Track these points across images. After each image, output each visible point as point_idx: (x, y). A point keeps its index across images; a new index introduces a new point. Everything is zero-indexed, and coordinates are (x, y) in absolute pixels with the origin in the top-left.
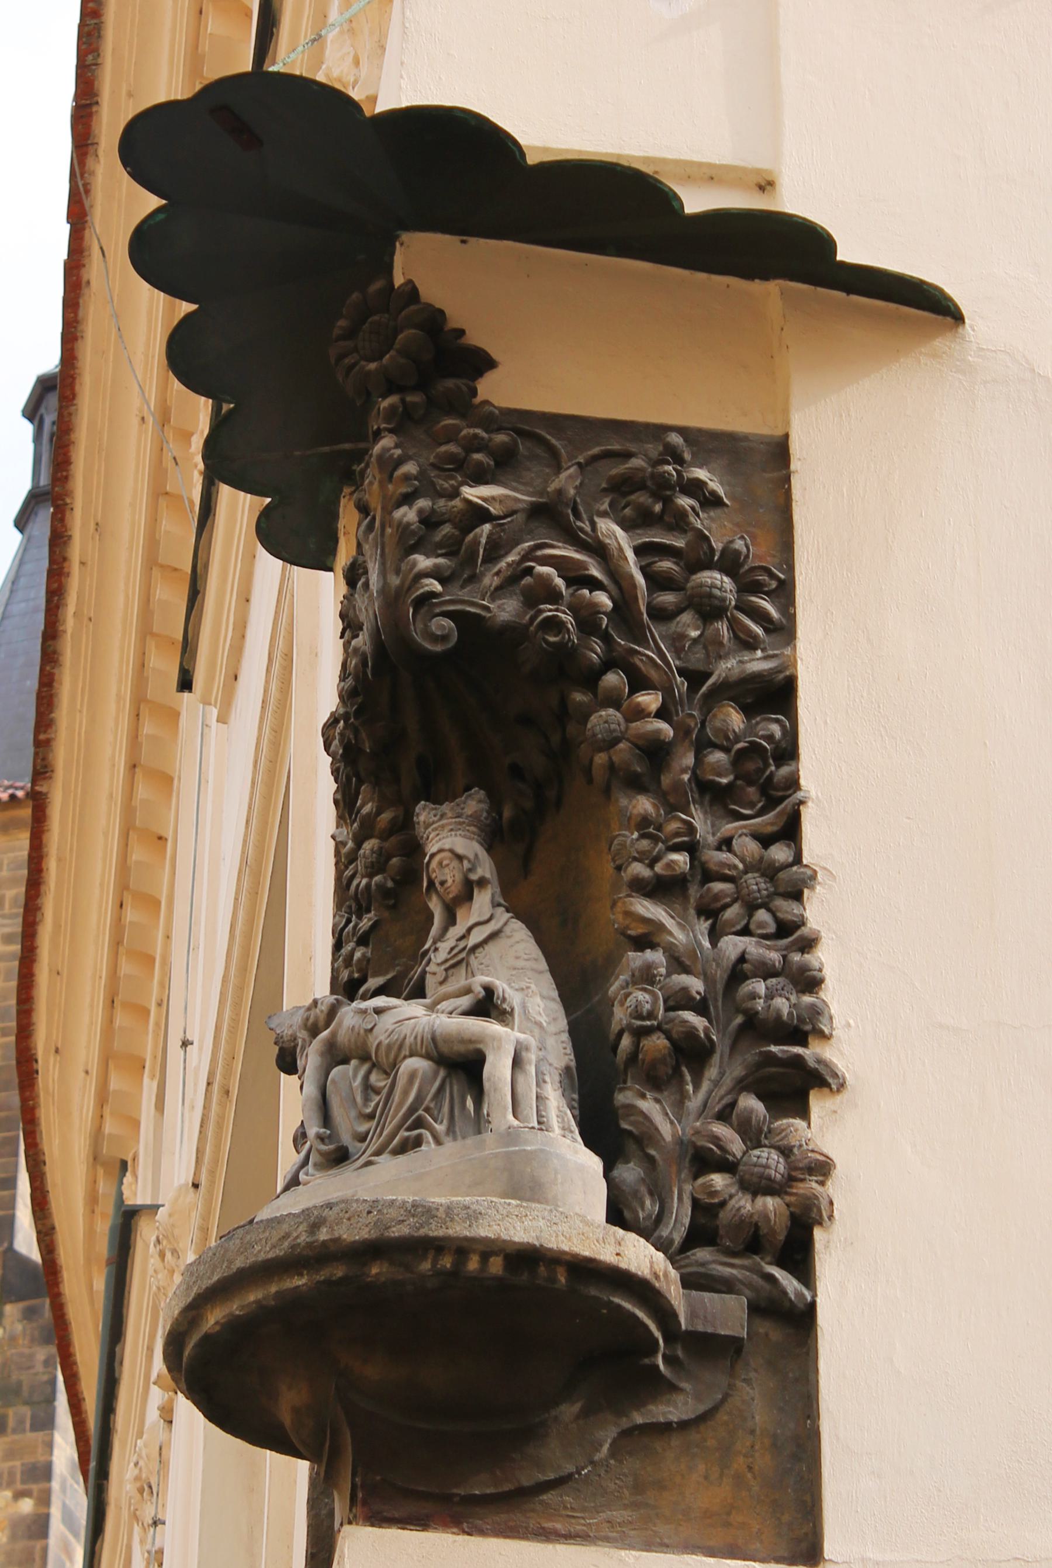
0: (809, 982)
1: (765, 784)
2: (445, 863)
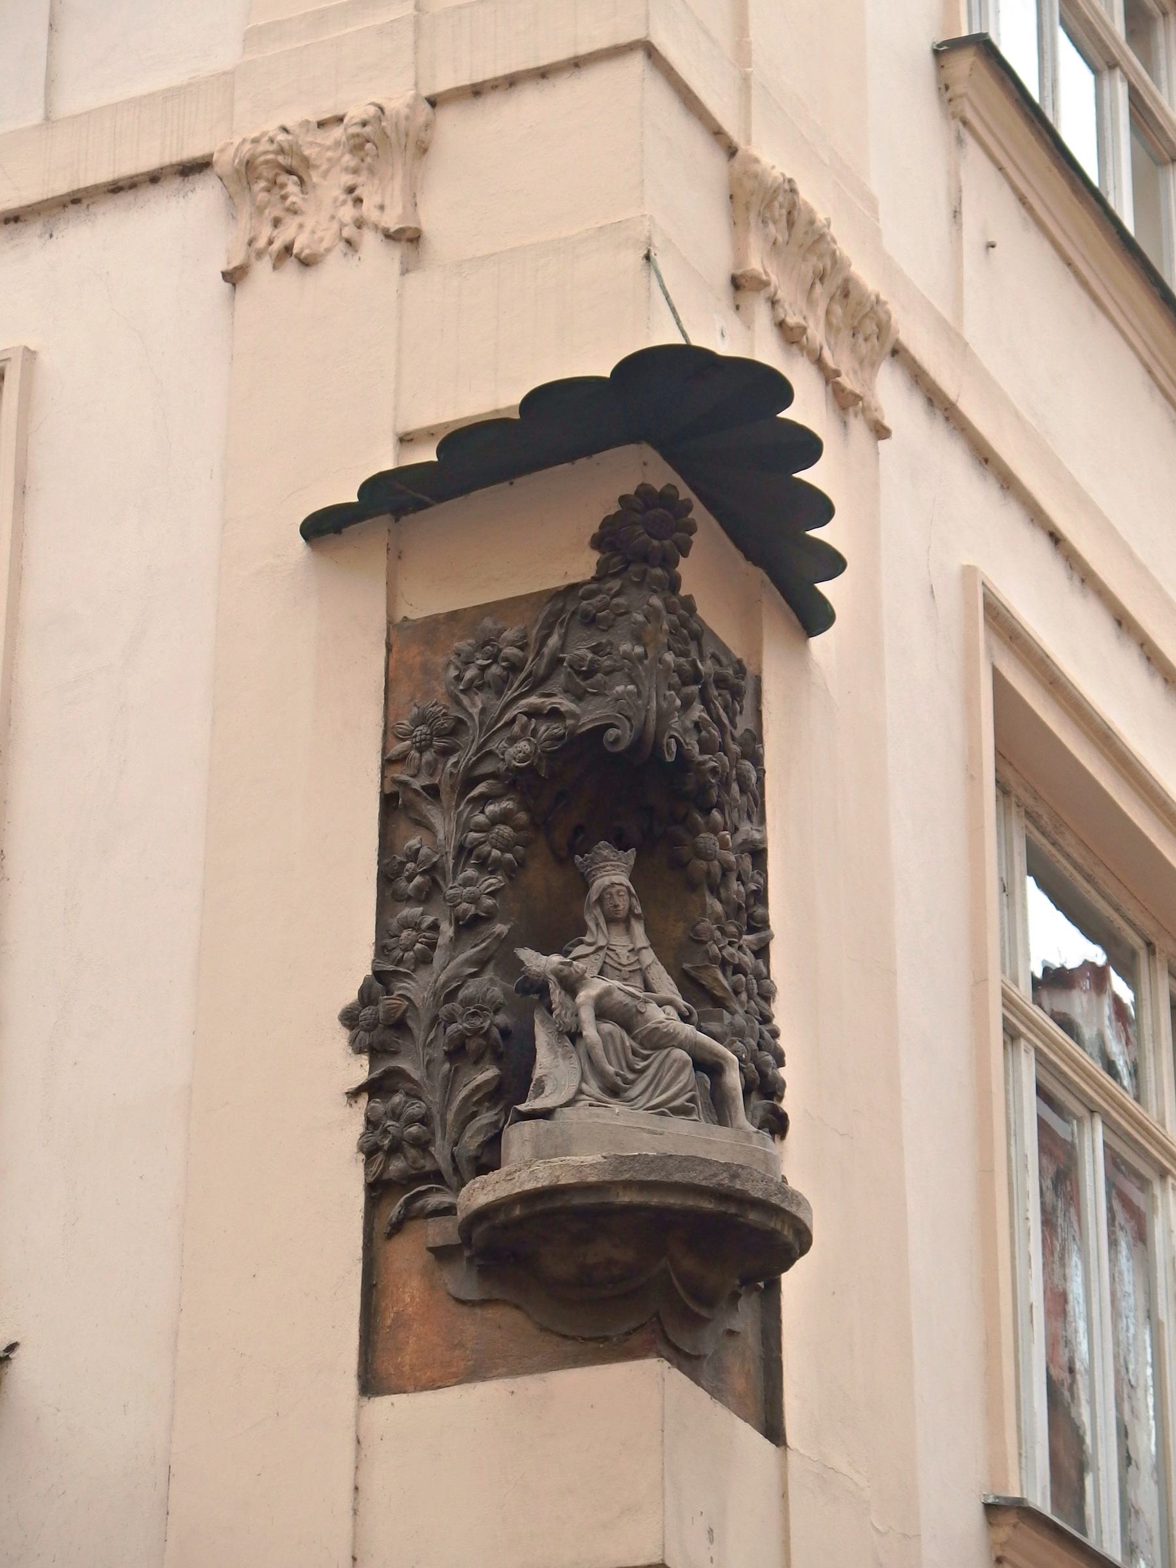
1: (752, 916)
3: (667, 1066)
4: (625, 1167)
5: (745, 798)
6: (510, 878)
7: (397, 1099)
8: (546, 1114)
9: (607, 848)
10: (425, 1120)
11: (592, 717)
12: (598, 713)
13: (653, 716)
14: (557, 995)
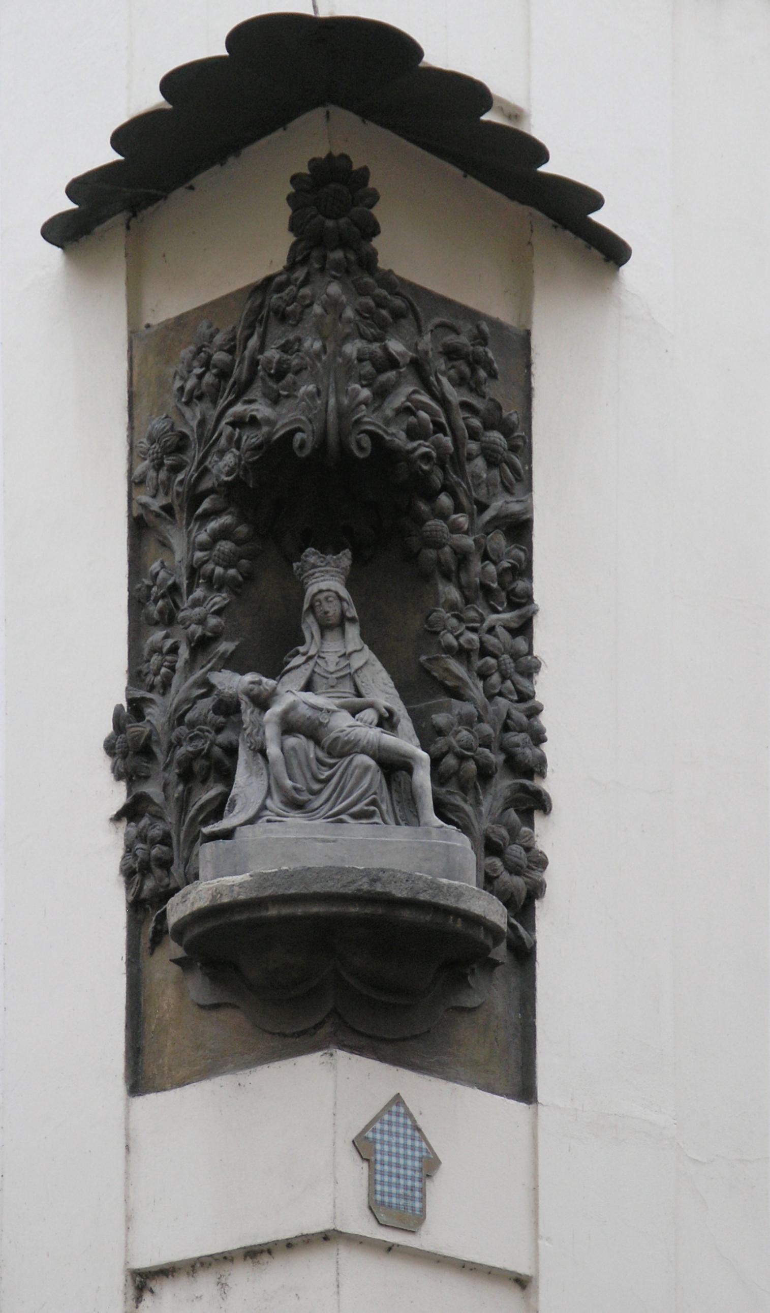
0: (539, 738)
1: (512, 592)
2: (330, 599)
3: (350, 771)
4: (268, 883)
5: (495, 472)
6: (236, 594)
7: (145, 821)
8: (228, 834)
9: (314, 554)
10: (166, 840)
11: (286, 420)
12: (291, 416)
13: (332, 418)
14: (248, 713)
